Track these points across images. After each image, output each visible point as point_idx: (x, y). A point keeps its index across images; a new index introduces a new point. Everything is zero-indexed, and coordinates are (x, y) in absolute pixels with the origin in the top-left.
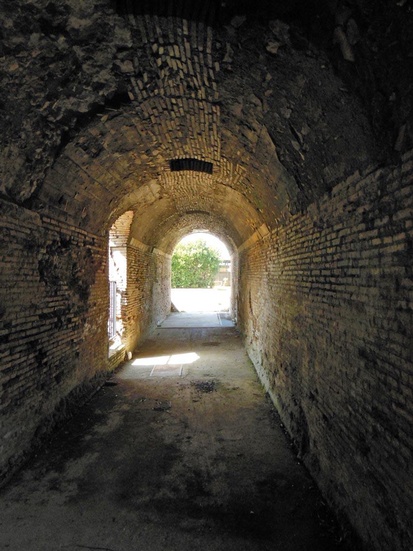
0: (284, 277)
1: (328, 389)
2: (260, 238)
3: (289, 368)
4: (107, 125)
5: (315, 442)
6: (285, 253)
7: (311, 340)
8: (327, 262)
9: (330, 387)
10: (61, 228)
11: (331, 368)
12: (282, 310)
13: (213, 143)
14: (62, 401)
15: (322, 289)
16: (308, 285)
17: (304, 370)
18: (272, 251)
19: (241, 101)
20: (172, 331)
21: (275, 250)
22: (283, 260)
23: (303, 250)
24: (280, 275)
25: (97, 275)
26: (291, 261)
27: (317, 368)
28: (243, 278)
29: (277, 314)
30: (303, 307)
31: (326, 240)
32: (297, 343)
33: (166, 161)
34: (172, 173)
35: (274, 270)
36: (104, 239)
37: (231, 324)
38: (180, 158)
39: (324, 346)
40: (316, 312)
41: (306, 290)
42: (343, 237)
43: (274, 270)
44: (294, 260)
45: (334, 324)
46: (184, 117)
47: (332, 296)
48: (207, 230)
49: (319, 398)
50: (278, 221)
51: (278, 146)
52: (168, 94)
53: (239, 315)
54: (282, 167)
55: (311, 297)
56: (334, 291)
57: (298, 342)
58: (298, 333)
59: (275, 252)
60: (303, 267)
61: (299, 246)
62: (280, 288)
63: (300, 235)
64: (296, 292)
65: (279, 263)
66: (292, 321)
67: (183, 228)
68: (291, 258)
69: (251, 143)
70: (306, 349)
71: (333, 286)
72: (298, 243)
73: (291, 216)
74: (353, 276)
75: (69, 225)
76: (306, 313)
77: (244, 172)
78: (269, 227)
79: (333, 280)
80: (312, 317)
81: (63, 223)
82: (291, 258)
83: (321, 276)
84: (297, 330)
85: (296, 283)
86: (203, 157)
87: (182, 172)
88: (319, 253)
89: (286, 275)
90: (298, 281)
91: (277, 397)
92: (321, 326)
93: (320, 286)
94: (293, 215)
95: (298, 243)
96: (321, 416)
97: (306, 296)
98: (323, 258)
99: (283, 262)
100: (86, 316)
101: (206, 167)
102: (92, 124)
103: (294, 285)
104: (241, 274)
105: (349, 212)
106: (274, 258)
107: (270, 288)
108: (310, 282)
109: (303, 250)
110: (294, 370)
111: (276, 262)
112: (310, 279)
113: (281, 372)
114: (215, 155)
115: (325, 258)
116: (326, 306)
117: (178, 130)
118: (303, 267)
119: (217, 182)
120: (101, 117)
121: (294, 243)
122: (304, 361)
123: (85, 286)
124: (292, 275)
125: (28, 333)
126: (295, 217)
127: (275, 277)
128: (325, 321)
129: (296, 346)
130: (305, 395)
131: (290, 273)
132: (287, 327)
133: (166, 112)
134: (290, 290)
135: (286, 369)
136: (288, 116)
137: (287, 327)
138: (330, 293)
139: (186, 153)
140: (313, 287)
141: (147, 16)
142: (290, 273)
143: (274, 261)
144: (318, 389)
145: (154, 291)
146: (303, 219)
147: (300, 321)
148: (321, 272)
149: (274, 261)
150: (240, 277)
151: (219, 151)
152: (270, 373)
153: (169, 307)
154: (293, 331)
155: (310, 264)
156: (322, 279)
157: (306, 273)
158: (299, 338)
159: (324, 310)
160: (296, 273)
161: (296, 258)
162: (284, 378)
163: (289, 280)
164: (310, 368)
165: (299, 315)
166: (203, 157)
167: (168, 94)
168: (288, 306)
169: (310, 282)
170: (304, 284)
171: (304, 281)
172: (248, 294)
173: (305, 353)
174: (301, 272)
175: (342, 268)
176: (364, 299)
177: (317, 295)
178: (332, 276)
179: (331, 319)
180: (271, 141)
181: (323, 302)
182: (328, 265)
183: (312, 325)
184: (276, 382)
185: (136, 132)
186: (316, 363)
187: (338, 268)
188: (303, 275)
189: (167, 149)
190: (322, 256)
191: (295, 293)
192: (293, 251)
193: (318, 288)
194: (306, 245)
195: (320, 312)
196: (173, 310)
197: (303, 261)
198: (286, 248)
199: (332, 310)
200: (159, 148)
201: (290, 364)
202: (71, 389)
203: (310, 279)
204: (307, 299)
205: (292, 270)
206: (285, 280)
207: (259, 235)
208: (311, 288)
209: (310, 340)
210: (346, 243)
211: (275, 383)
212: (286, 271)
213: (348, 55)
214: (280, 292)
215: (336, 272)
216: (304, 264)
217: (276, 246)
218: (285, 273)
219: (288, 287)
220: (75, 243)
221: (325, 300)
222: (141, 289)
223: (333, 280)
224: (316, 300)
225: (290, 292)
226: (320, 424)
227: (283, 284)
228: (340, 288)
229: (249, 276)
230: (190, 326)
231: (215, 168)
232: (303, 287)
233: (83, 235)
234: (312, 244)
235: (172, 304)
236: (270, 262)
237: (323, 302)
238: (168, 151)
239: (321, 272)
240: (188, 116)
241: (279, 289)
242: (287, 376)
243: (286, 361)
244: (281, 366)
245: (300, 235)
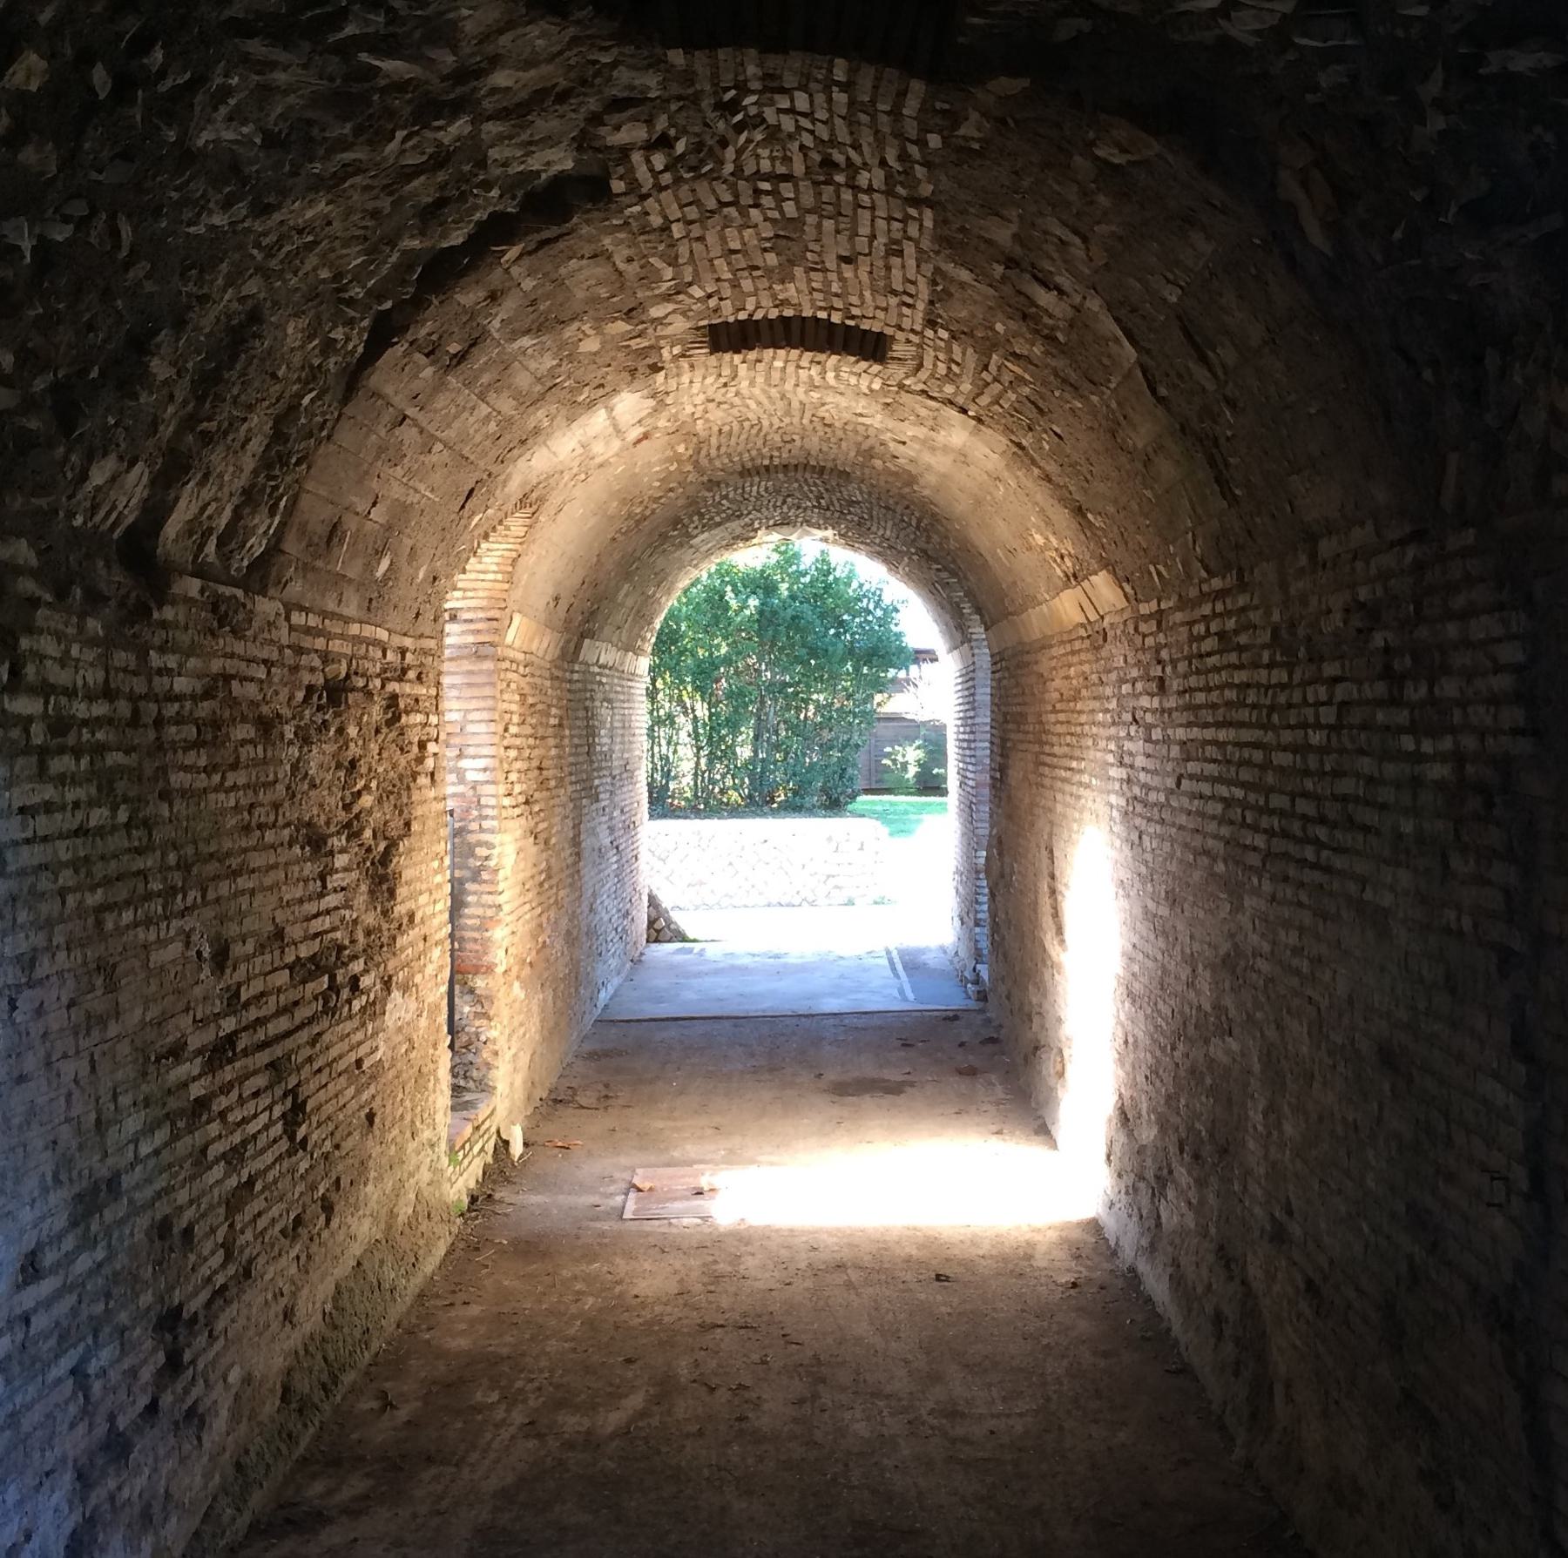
0: (1185, 801)
1: (1316, 1187)
2: (1093, 617)
3: (1207, 1150)
4: (515, 271)
7: (1272, 1033)
8: (1306, 773)
9: (1321, 1181)
11: (1321, 1119)
12: (1180, 927)
14: (337, 1286)
15: (1297, 861)
16: (1260, 840)
17: (1251, 1145)
18: (1139, 686)
19: (1015, 219)
20: (700, 1028)
21: (1154, 686)
22: (1181, 733)
23: (1244, 715)
24: (1172, 792)
25: (416, 796)
27: (1288, 1128)
29: (1161, 943)
30: (1244, 919)
32: (1228, 1052)
33: (698, 329)
34: (713, 360)
35: (1150, 764)
37: (954, 999)
39: (1305, 1049)
40: (1282, 933)
43: (1150, 764)
44: (1215, 743)
45: (1327, 977)
46: (797, 222)
47: (1321, 886)
48: (829, 533)
49: (1296, 1230)
50: (1159, 574)
51: (1148, 352)
52: (749, 169)
53: (998, 944)
54: (1160, 412)
55: (1267, 887)
56: (1328, 870)
57: (1234, 1045)
58: (1232, 1013)
59: (1152, 695)
60: (1246, 775)
61: (1231, 694)
62: (1172, 841)
64: (1225, 861)
65: (1166, 741)
66: (1210, 966)
67: (711, 528)
70: (1257, 1068)
71: (1325, 854)
73: (1204, 574)
74: (1366, 829)
77: (1021, 380)
78: (1128, 588)
79: (1322, 833)
80: (1272, 952)
82: (1209, 734)
83: (1293, 815)
84: (1228, 1001)
85: (1225, 831)
86: (853, 317)
87: (752, 355)
90: (1232, 823)
91: (1170, 1270)
92: (1295, 981)
93: (1292, 848)
95: (1230, 685)
96: (1302, 1286)
97: (1255, 881)
98: (1298, 757)
99: (1183, 743)
102: (473, 277)
103: (1216, 837)
104: (1004, 755)
105: (1360, 631)
106: (1149, 718)
107: (1135, 836)
108: (1265, 831)
109: (1244, 715)
110: (1224, 1151)
111: (1157, 734)
112: (1265, 822)
115: (1304, 759)
116: (1307, 918)
119: (901, 386)
120: (504, 253)
122: (1251, 1113)
124: (1213, 797)
126: (1217, 583)
128: (1305, 967)
129: (1225, 1059)
130: (1257, 1233)
134: (1206, 853)
135: (1196, 1157)
136: (1174, 299)
138: (1317, 876)
139: (785, 303)
141: (722, 54)
145: (587, 843)
147: (1238, 970)
148: (1293, 801)
149: (1149, 728)
150: (1003, 769)
151: (921, 306)
152: (1142, 1185)
153: (642, 916)
154: (1217, 1007)
155: (1264, 767)
157: (1252, 797)
158: (1236, 1031)
160: (1223, 791)
161: (1222, 735)
165: (1236, 946)
166: (853, 317)
168: (1201, 914)
169: (1265, 831)
172: (1044, 853)
173: (1254, 1084)
175: (1344, 799)
177: (1286, 879)
178: (1322, 820)
180: (1120, 333)
182: (1309, 785)
185: (610, 268)
186: (1286, 1108)
187: (1335, 798)
188: (1244, 805)
189: (710, 296)
191: (1220, 867)
194: (1252, 697)
195: (1292, 939)
197: (1246, 753)
198: (1191, 690)
200: (681, 297)
201: (1212, 1135)
202: (358, 1253)
204: (1256, 892)
205: (1213, 780)
206: (1189, 813)
207: (1086, 604)
209: (1267, 1033)
211: (1159, 1225)
212: (1191, 777)
213: (1317, 237)
218: (1185, 783)
219: (1197, 842)
220: (360, 683)
221: (1304, 898)
222: (542, 837)
223: (1322, 833)
224: (1280, 895)
226: (1299, 1316)
227: (1181, 828)
228: (1339, 862)
229: (1046, 770)
230: (753, 1008)
231: (899, 349)
232: (1246, 846)
234: (1268, 702)
235: (653, 902)
237: (1300, 904)
238: (713, 303)
239: (1293, 801)
241: (1167, 846)
243: (1198, 1126)
244: (1182, 1151)
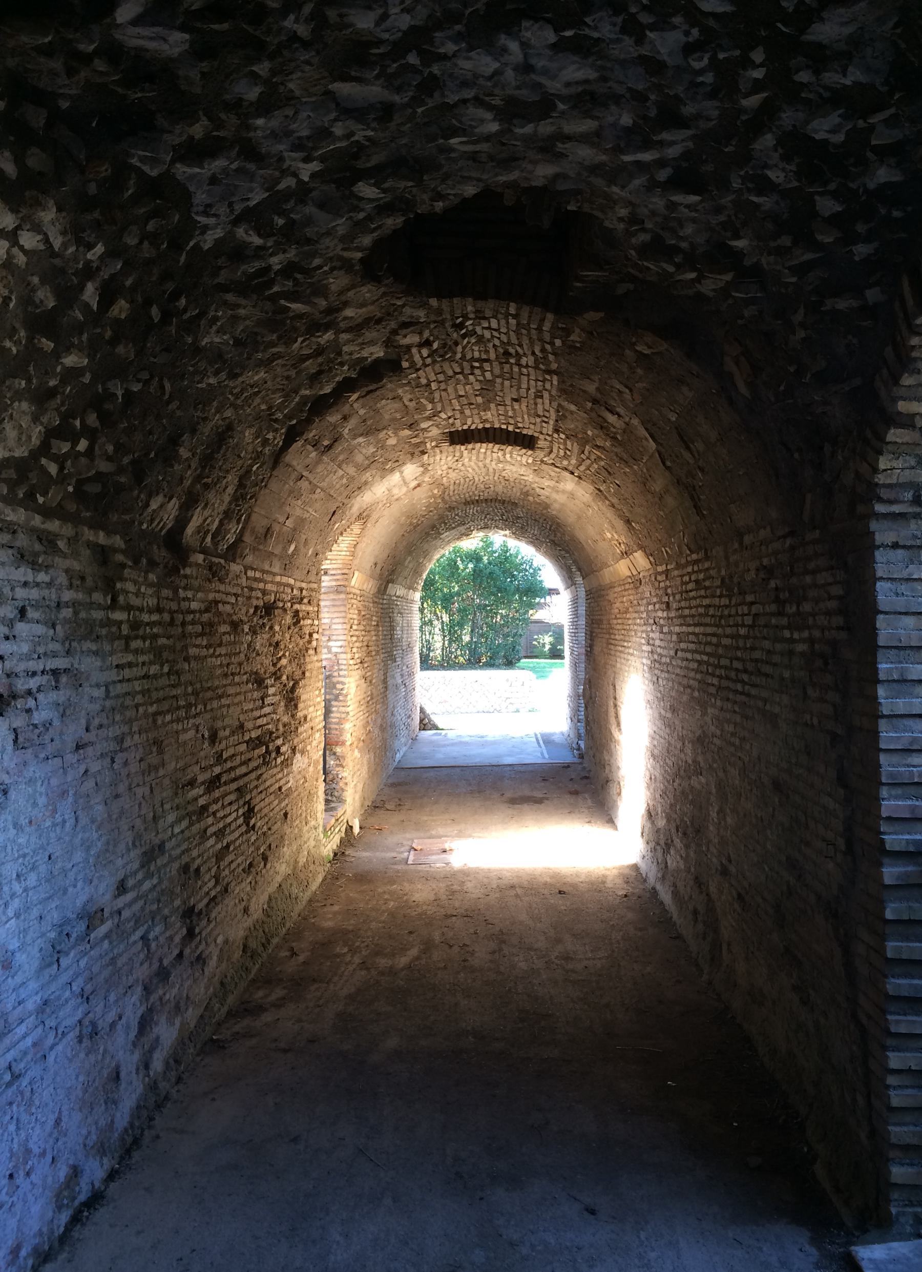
0: (679, 662)
1: (743, 848)
2: (635, 573)
4: (356, 405)
5: (729, 945)
6: (680, 617)
8: (738, 648)
9: (745, 846)
10: (266, 582)
11: (745, 815)
13: (540, 413)
17: (711, 828)
21: (664, 606)
22: (677, 629)
24: (673, 657)
25: (307, 659)
26: (689, 633)
27: (729, 820)
28: (597, 649)
29: (668, 730)
30: (708, 719)
31: (737, 614)
32: (700, 783)
36: (315, 586)
38: (473, 427)
39: (737, 782)
40: (726, 726)
41: (712, 690)
42: (756, 615)
45: (748, 747)
46: (492, 382)
48: (507, 532)
49: (732, 869)
51: (661, 445)
52: (469, 356)
53: (589, 731)
56: (748, 695)
59: (663, 611)
60: (709, 649)
61: (702, 610)
62: (673, 681)
63: (702, 592)
64: (699, 691)
65: (670, 633)
66: (692, 742)
67: (450, 530)
68: (691, 629)
69: (614, 427)
70: (714, 791)
72: (701, 606)
73: (688, 552)
75: (275, 575)
76: (713, 728)
78: (651, 559)
79: (745, 677)
81: (268, 572)
82: (691, 629)
83: (731, 668)
84: (700, 758)
86: (519, 428)
88: (729, 631)
89: (683, 659)
90: (702, 672)
92: (732, 749)
93: (731, 685)
94: (692, 552)
95: (701, 606)
97: (713, 700)
100: (296, 741)
101: (528, 442)
103: (694, 679)
105: (763, 579)
106: (662, 622)
110: (698, 831)
111: (665, 629)
112: (718, 672)
113: (678, 842)
114: (542, 427)
116: (738, 719)
117: (476, 395)
118: (709, 649)
119: (542, 461)
120: (350, 397)
121: (694, 603)
123: (291, 684)
125: (238, 772)
127: (664, 660)
128: (737, 742)
130: (714, 871)
131: (689, 656)
132: (686, 755)
133: (460, 377)
134: (689, 687)
135: (685, 834)
136: (674, 419)
137: (686, 755)
138: (743, 698)
139: (486, 421)
140: (722, 685)
141: (455, 300)
142: (689, 656)
143: (662, 626)
144: (732, 856)
145: (390, 682)
146: (707, 565)
147: (705, 744)
148: (731, 662)
151: (552, 422)
152: (658, 848)
154: (694, 761)
156: (733, 674)
157: (711, 660)
158: (704, 773)
159: (736, 724)
160: (698, 657)
161: (697, 630)
162: (682, 852)
163: (687, 668)
164: (720, 823)
167: (469, 356)
168: (687, 717)
169: (718, 676)
170: (710, 680)
171: (710, 674)
173: (713, 799)
174: (705, 658)
175: (756, 661)
176: (777, 710)
177: (728, 700)
179: (744, 739)
181: (735, 712)
182: (739, 654)
183: (721, 748)
184: (669, 863)
188: (708, 664)
190: (732, 637)
191: (696, 694)
192: (693, 616)
193: (728, 688)
194: (711, 612)
196: (426, 724)
197: (709, 639)
199: (745, 723)
201: (692, 824)
203: (718, 672)
204: (714, 706)
206: (681, 668)
208: (719, 688)
210: (760, 626)
211: (666, 867)
212: (682, 650)
214: (673, 688)
215: (750, 666)
216: (710, 643)
217: (666, 599)
219: (685, 681)
220: (281, 605)
222: (368, 679)
223: (745, 677)
225: (689, 691)
227: (677, 675)
228: (753, 691)
229: (612, 647)
230: (477, 761)
231: (541, 443)
233: (288, 585)
234: (719, 614)
235: (422, 710)
236: (654, 627)
237: (735, 712)
238: (451, 421)
240: (499, 380)
242: (687, 847)
244: (678, 831)
245: (702, 592)
